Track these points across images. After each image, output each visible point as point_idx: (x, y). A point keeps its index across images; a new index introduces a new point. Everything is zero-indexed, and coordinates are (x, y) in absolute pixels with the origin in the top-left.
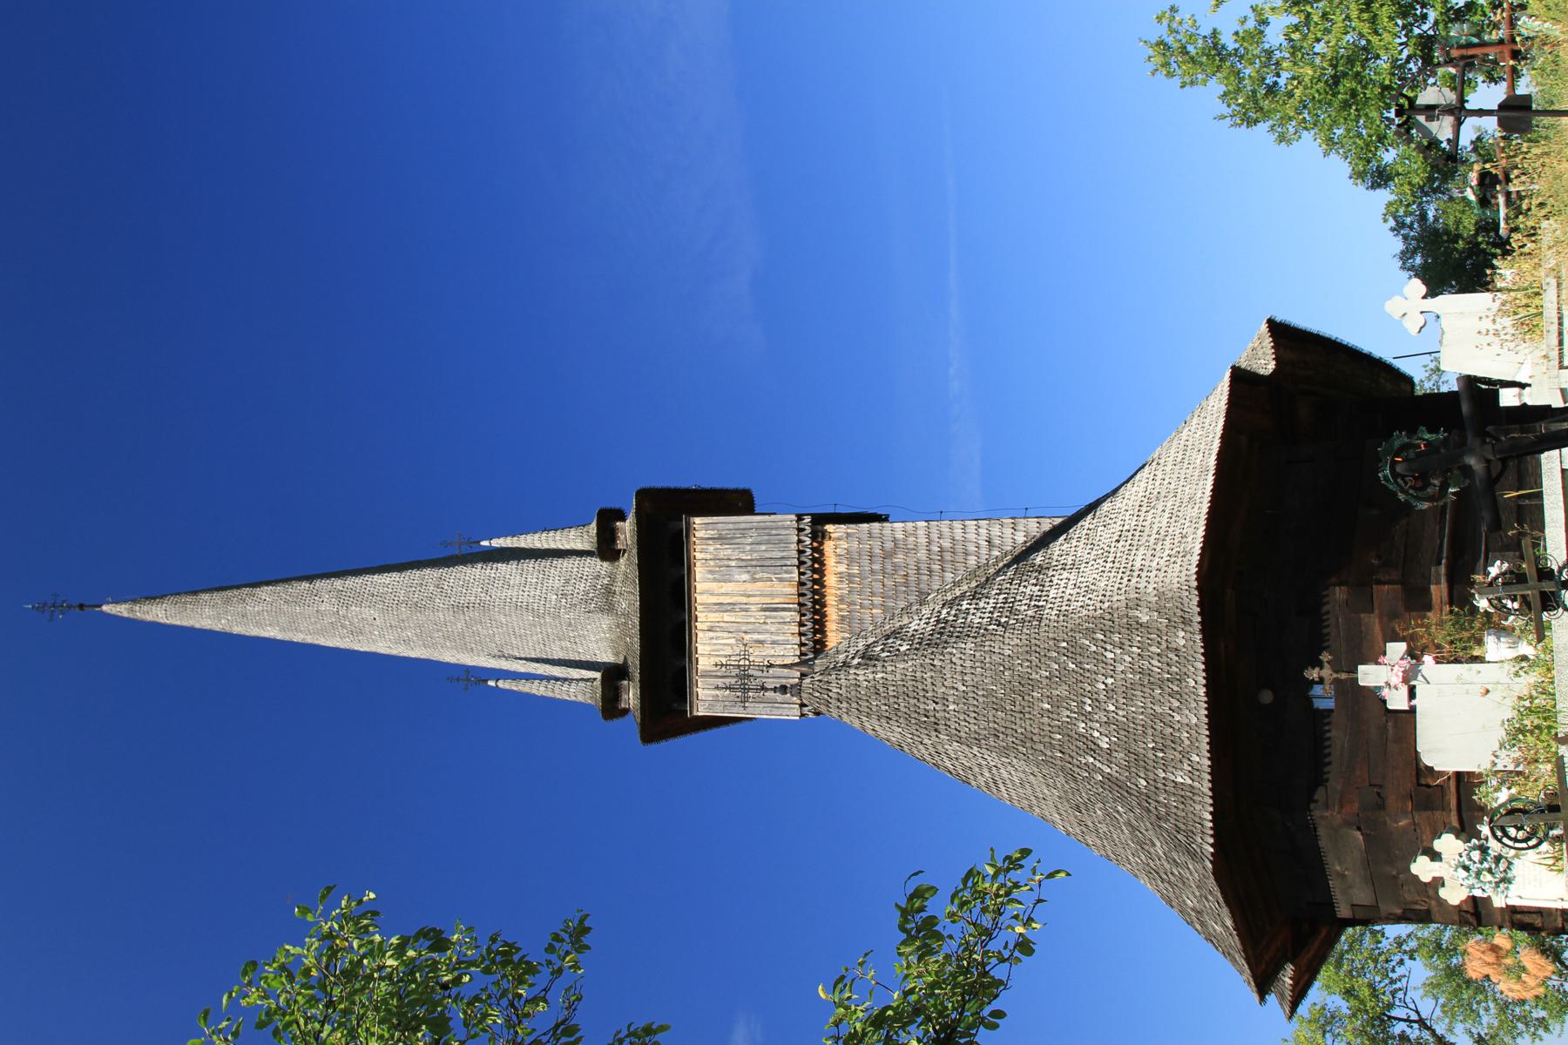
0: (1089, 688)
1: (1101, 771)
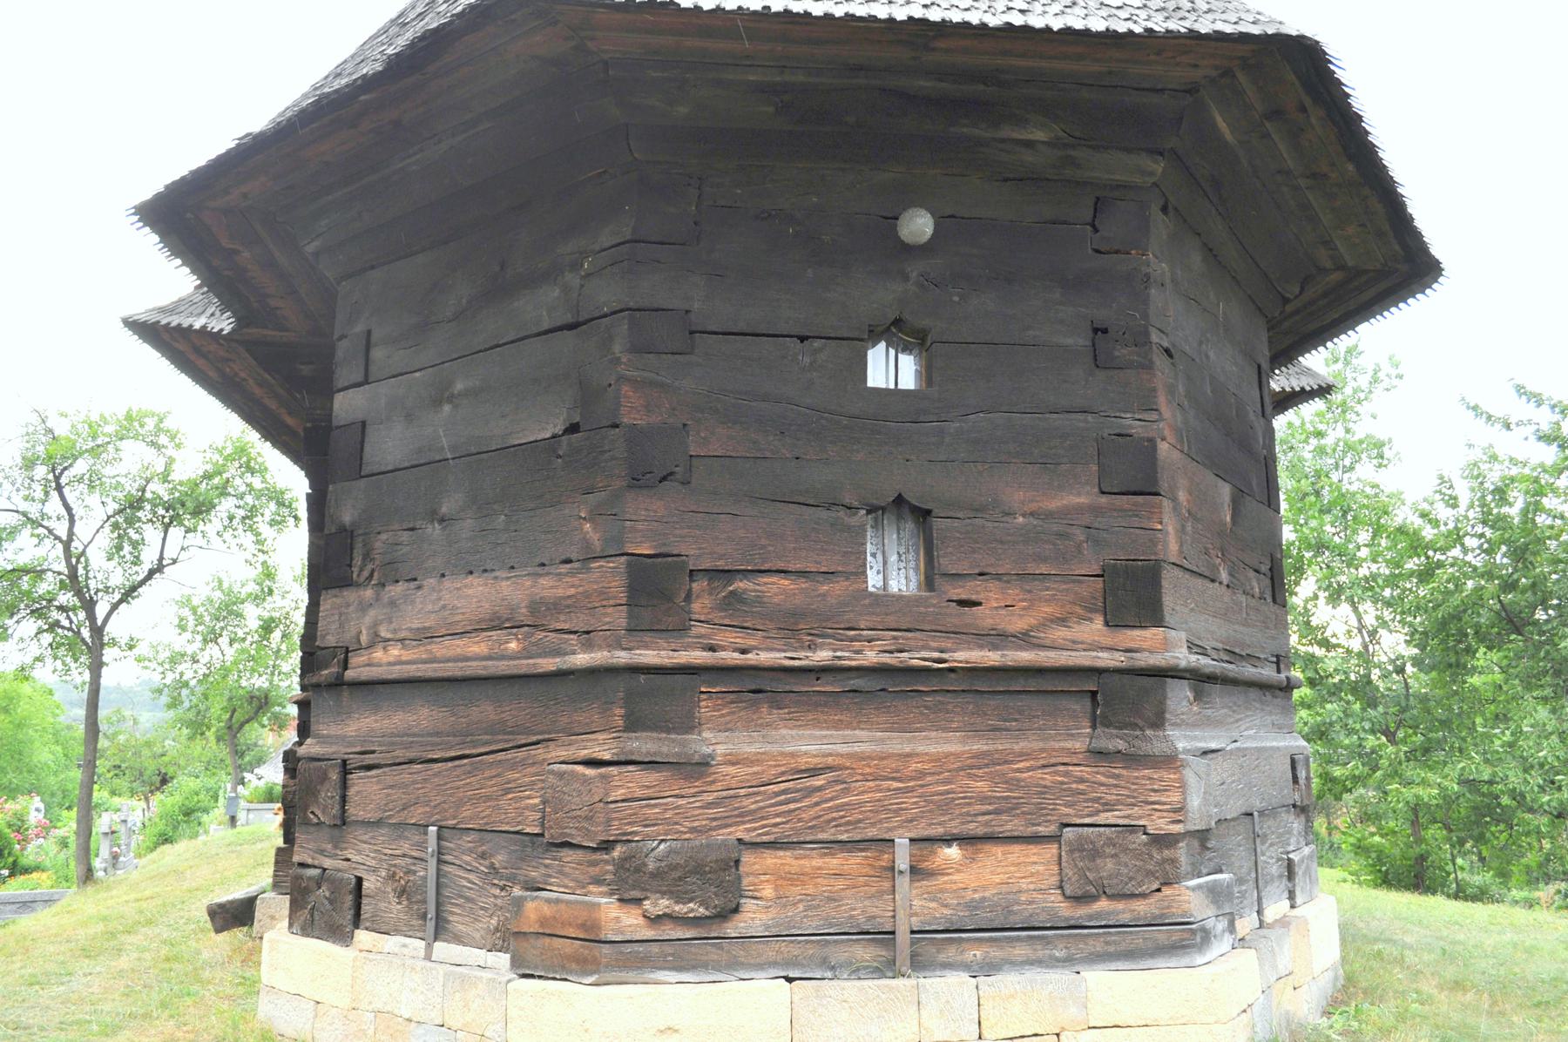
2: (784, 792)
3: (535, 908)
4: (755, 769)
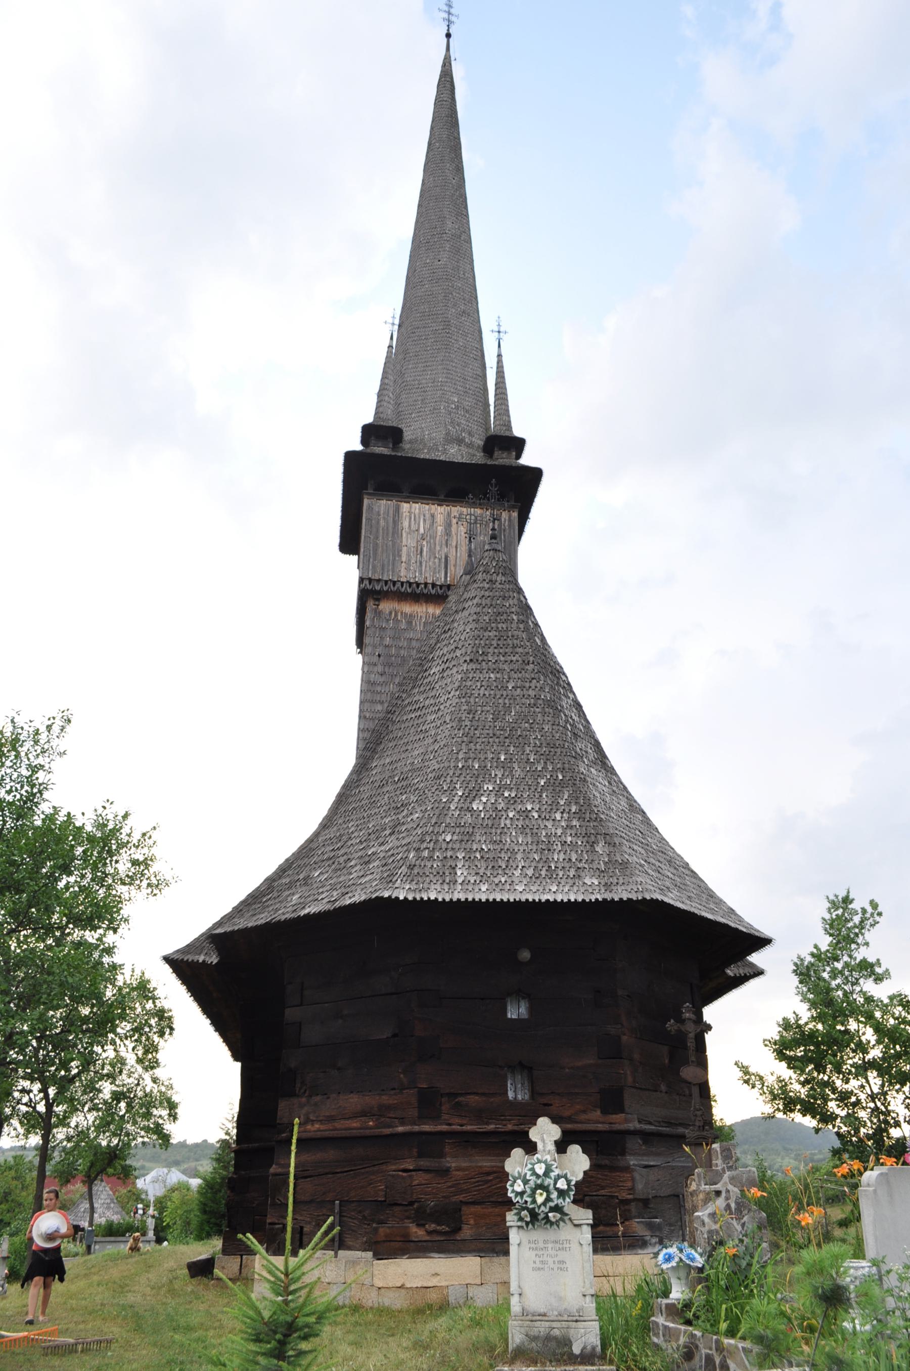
0: (525, 796)
1: (450, 801)
3: (383, 1231)
4: (467, 1173)
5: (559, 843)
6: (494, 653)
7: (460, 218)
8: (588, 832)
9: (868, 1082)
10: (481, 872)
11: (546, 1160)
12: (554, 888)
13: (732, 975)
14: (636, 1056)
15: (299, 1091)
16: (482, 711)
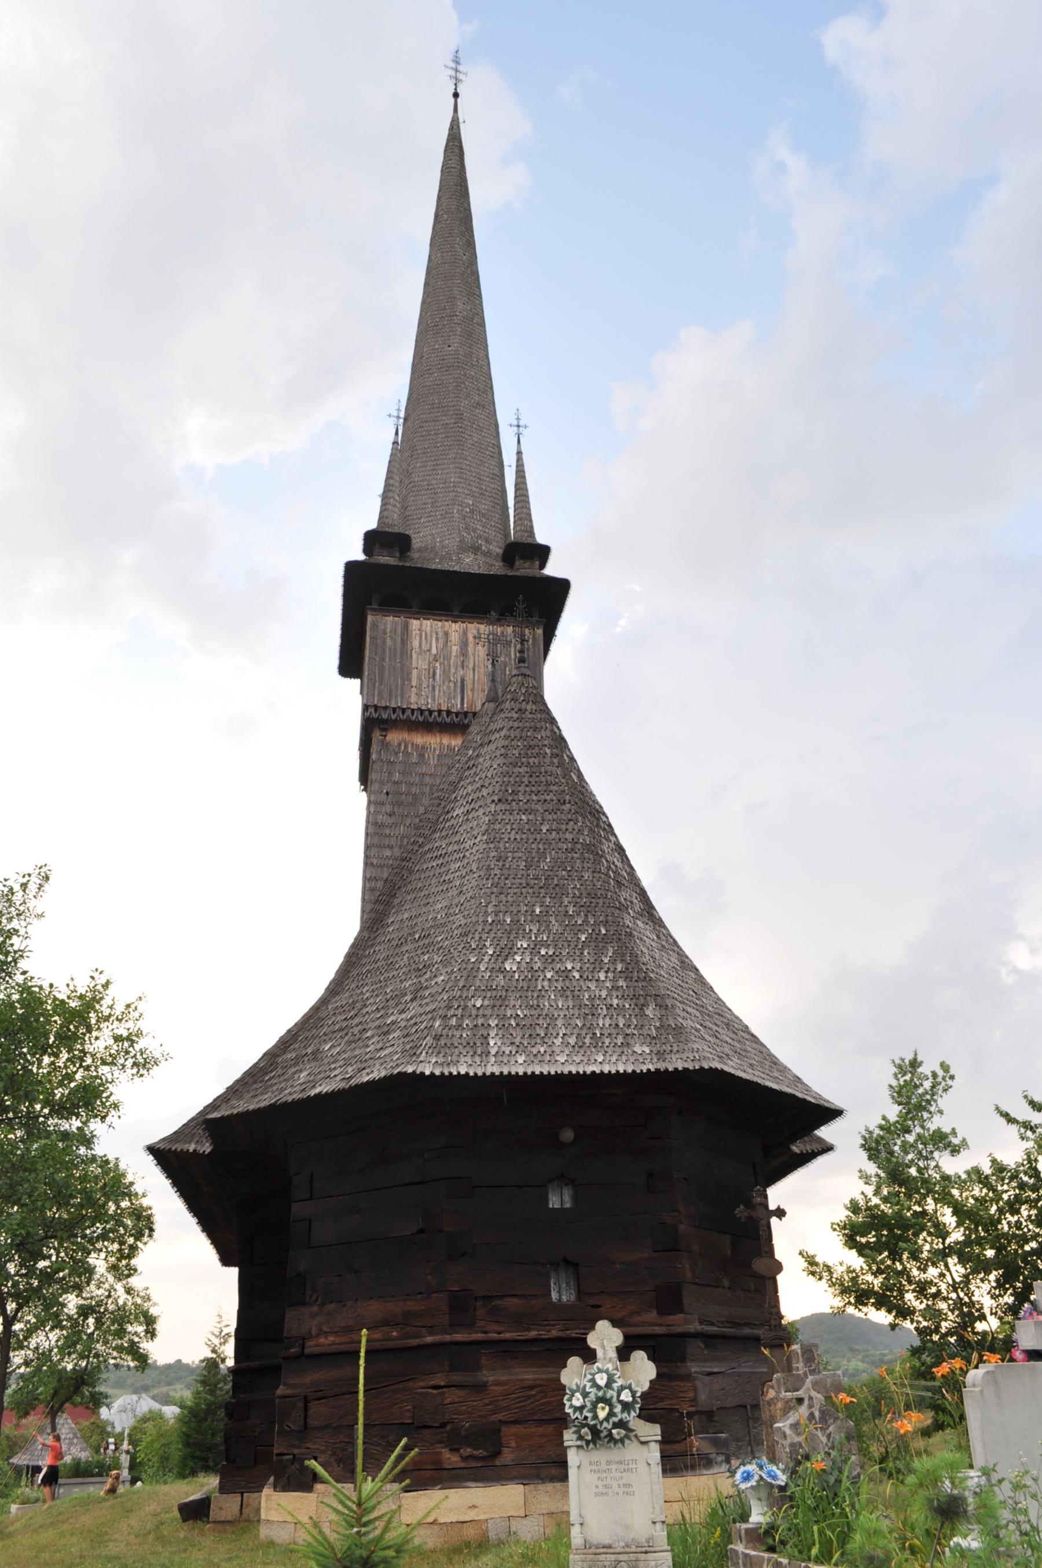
0: (564, 954)
1: (479, 961)
2: (519, 1397)
4: (505, 1387)
5: (604, 1007)
6: (525, 791)
7: (472, 298)
8: (637, 994)
9: (949, 1270)
10: (517, 1041)
11: (608, 1369)
12: (600, 1058)
13: (798, 1152)
14: (695, 1248)
15: (310, 1299)
16: (514, 858)
